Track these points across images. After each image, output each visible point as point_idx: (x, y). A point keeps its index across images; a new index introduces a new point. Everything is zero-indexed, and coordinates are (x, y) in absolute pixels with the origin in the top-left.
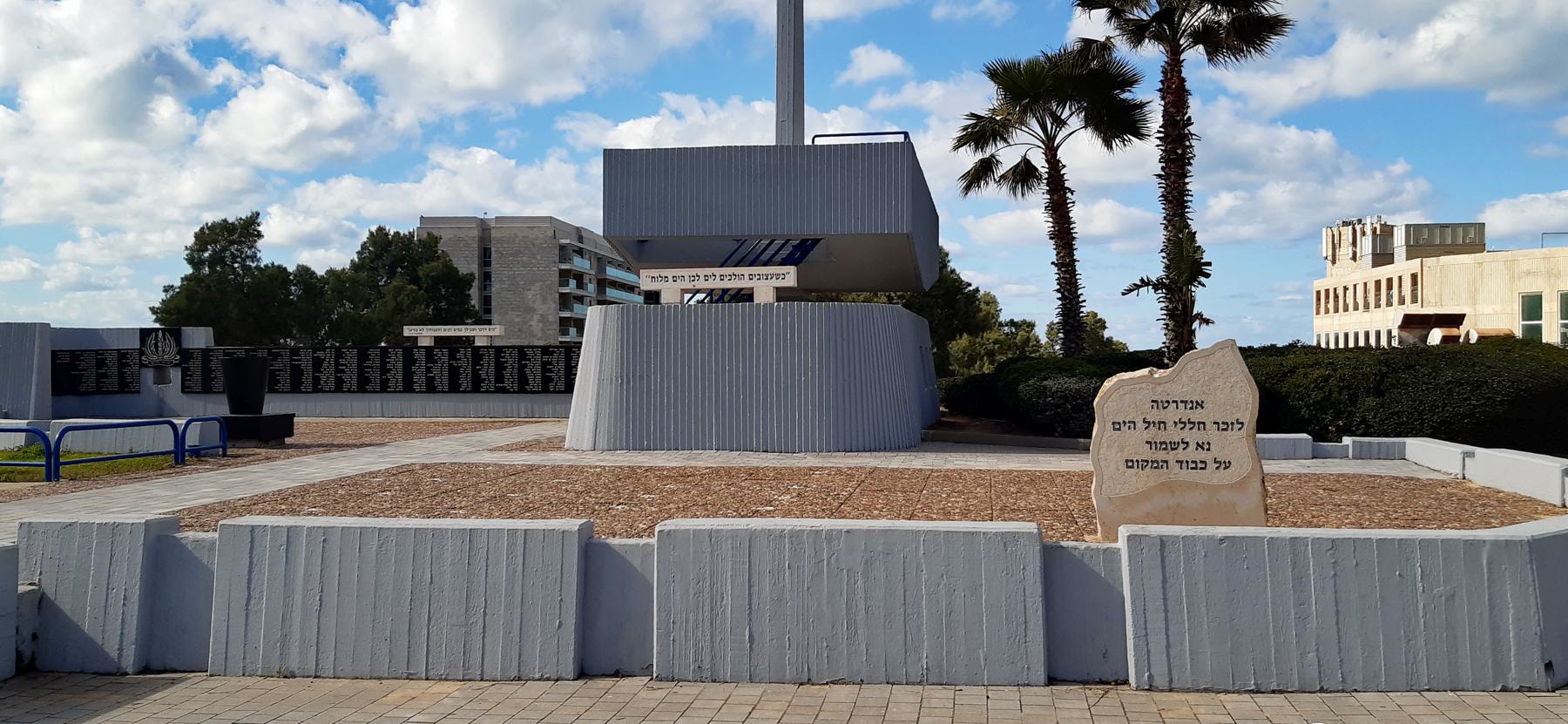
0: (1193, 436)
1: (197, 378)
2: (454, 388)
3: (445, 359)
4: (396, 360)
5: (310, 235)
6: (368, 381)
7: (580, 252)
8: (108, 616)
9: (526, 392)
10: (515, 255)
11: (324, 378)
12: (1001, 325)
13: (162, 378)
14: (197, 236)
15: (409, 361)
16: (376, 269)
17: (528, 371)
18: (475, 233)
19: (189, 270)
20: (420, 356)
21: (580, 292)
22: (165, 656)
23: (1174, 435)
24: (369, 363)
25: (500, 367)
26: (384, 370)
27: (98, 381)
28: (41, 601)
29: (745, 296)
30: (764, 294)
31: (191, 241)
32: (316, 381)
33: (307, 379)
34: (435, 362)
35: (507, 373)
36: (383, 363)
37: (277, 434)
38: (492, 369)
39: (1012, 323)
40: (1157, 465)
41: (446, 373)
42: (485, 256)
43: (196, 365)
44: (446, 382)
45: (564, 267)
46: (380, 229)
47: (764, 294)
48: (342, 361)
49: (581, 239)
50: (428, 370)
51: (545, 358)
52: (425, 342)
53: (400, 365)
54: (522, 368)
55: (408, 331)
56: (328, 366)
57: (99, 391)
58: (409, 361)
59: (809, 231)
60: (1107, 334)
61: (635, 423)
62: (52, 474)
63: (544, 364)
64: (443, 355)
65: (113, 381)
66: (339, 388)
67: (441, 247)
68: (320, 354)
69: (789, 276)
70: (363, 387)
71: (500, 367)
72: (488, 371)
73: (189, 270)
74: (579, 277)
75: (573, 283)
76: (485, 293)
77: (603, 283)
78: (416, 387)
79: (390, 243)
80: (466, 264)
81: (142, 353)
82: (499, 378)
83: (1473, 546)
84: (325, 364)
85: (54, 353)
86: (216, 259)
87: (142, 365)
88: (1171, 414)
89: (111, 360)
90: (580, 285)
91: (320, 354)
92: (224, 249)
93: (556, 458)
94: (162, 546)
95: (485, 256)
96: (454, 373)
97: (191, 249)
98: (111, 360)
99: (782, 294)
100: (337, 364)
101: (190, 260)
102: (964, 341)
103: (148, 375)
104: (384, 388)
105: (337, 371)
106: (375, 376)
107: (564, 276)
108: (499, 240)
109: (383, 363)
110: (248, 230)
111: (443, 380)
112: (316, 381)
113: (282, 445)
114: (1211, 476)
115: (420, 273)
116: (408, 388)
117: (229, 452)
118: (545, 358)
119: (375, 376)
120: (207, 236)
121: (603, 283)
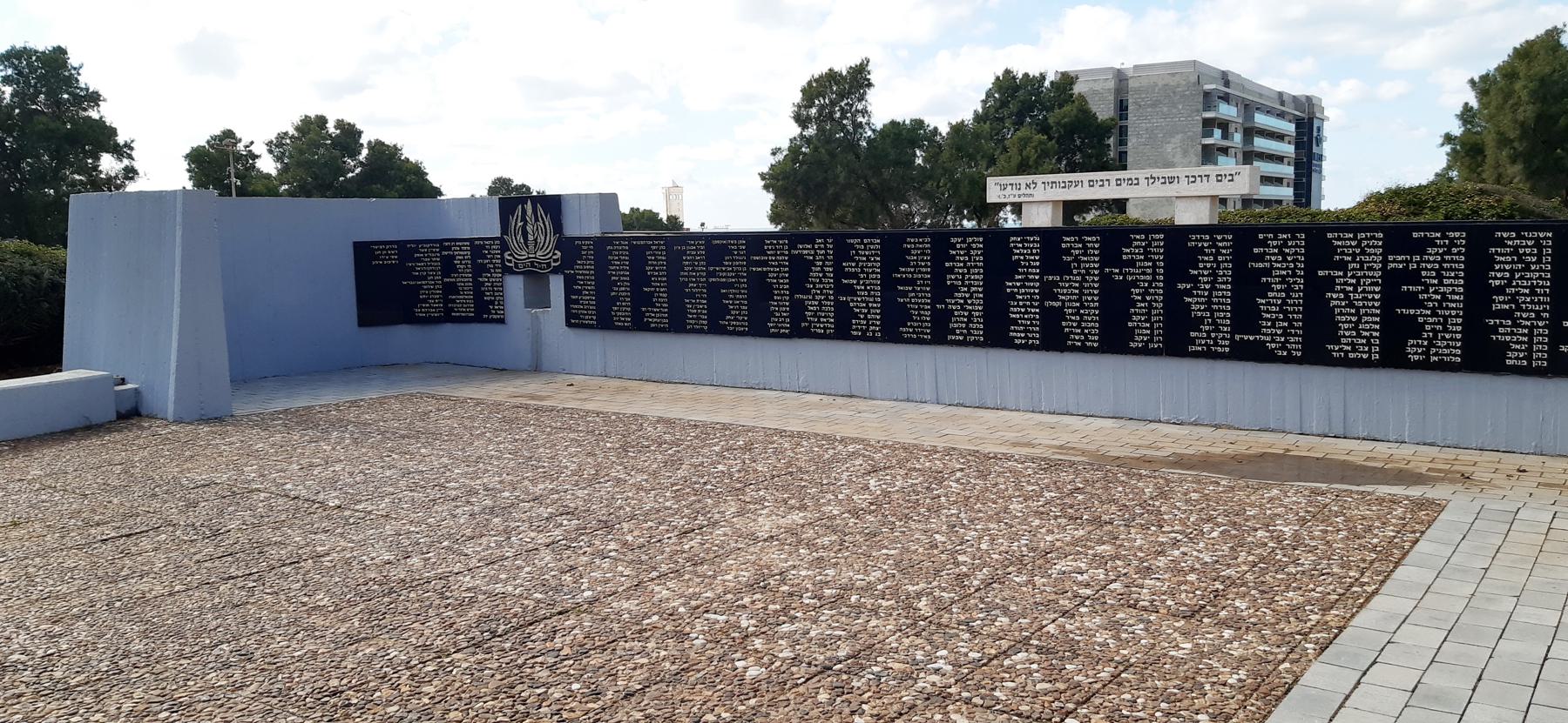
1: (588, 300)
2: (1115, 340)
3: (1093, 262)
6: (904, 315)
7: (1226, 98)
9: (1327, 360)
10: (1154, 105)
11: (812, 306)
13: (538, 299)
14: (804, 91)
16: (1002, 120)
17: (1335, 298)
18: (1111, 85)
19: (795, 130)
20: (1028, 255)
21: (1225, 143)
24: (904, 272)
25: (1248, 285)
26: (942, 290)
27: (446, 301)
32: (798, 310)
33: (780, 307)
34: (1065, 270)
35: (1268, 306)
36: (939, 273)
38: (1225, 290)
41: (1093, 300)
42: (1122, 107)
43: (585, 269)
44: (1093, 325)
45: (1208, 115)
46: (1007, 72)
48: (849, 267)
49: (1227, 84)
50: (1048, 292)
51: (1397, 262)
52: (1042, 217)
53: (977, 277)
54: (1316, 290)
57: (448, 317)
60: (625, 209)
63: (1392, 280)
65: (464, 302)
66: (842, 331)
67: (1077, 89)
68: (805, 250)
70: (893, 329)
71: (1248, 285)
72: (1210, 294)
73: (795, 130)
74: (1224, 126)
75: (1218, 133)
76: (1122, 149)
77: (1250, 132)
78: (1017, 334)
79: (1017, 88)
80: (1104, 111)
81: (504, 247)
82: (1246, 317)
84: (815, 273)
85: (359, 247)
87: (507, 271)
89: (462, 256)
90: (1225, 136)
91: (805, 250)
92: (833, 103)
95: (1122, 107)
96: (1116, 303)
97: (799, 107)
98: (462, 256)
100: (839, 273)
103: (515, 287)
104: (940, 334)
105: (841, 289)
106: (919, 300)
107: (1208, 124)
108: (1138, 91)
109: (939, 273)
110: (857, 80)
112: (798, 310)
115: (1051, 121)
116: (997, 335)
118: (1397, 262)
119: (919, 300)
120: (812, 91)
121: (1250, 132)
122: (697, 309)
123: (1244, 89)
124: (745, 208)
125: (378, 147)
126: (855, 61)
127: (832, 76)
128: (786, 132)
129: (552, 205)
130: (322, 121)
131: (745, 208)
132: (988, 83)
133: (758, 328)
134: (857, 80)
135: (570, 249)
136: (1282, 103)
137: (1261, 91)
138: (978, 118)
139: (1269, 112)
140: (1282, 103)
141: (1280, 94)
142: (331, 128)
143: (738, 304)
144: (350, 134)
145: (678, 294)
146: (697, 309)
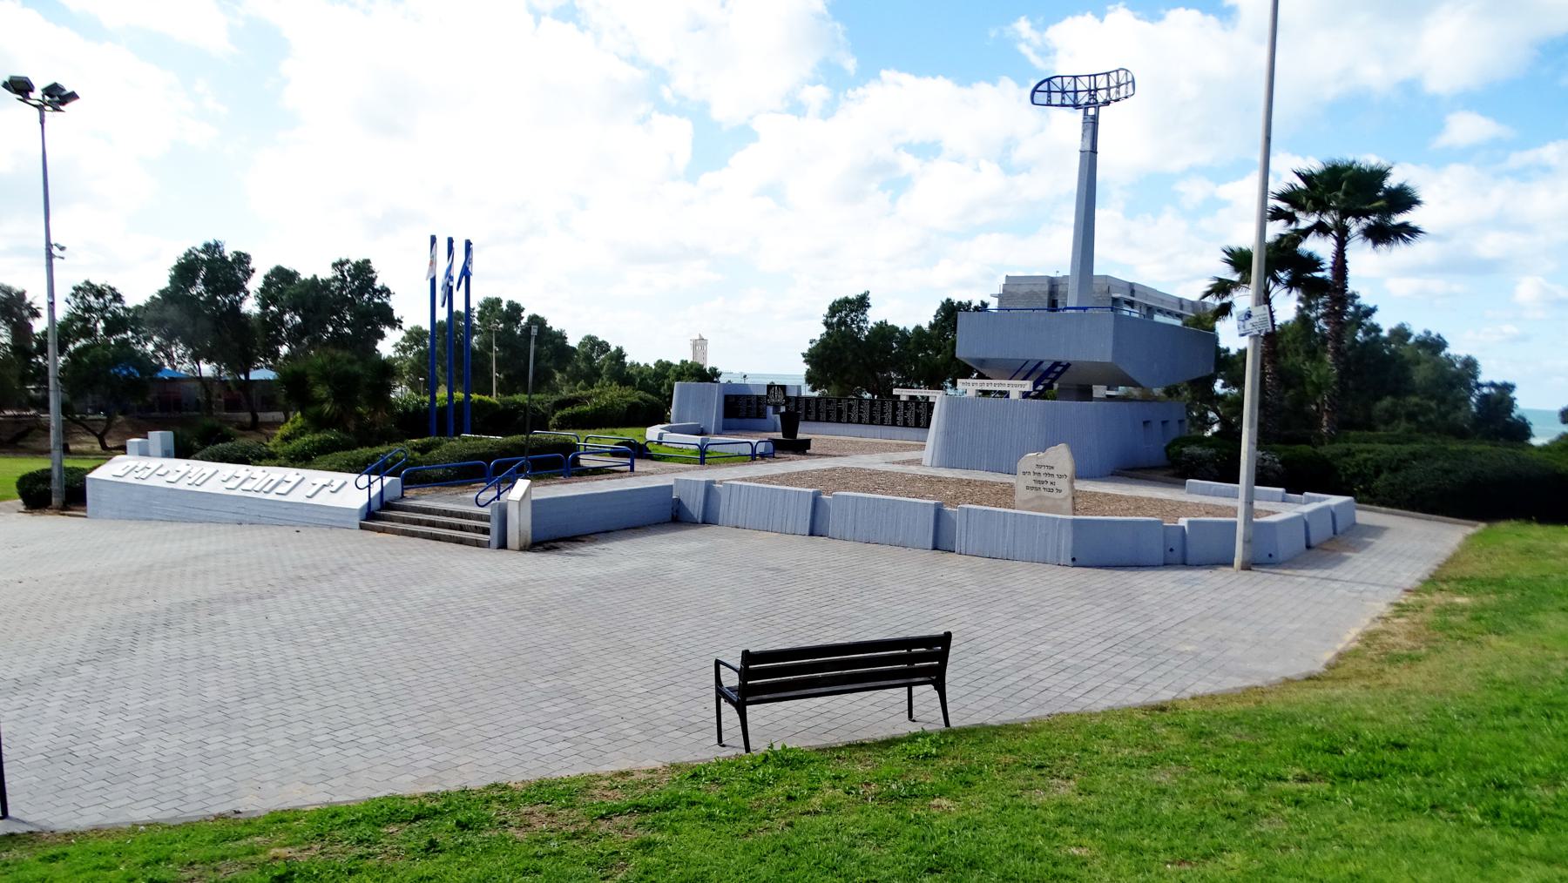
0: (1049, 479)
4: (889, 406)
5: (904, 308)
7: (1131, 304)
8: (695, 507)
12: (1479, 386)
15: (895, 408)
18: (1046, 288)
20: (901, 406)
22: (708, 519)
23: (1043, 478)
26: (883, 413)
28: (679, 501)
29: (1005, 394)
30: (1015, 394)
31: (826, 311)
33: (845, 416)
37: (802, 448)
39: (1493, 385)
40: (1038, 489)
47: (1015, 394)
49: (1133, 293)
52: (903, 398)
55: (895, 392)
56: (855, 409)
57: (747, 417)
58: (895, 408)
59: (1062, 357)
61: (950, 457)
62: (702, 462)
64: (912, 406)
66: (860, 422)
69: (1028, 386)
70: (871, 422)
73: (824, 329)
83: (1055, 519)
86: (842, 322)
88: (1043, 471)
93: (913, 469)
94: (709, 487)
99: (1026, 395)
101: (826, 323)
102: (1387, 402)
103: (770, 409)
104: (882, 423)
110: (862, 303)
111: (912, 421)
113: (804, 453)
114: (1055, 495)
116: (894, 424)
117: (636, 468)
120: (835, 308)
122: (823, 416)
123: (1147, 297)
124: (792, 370)
125: (534, 319)
126: (861, 292)
127: (847, 301)
128: (818, 331)
129: (783, 388)
130: (499, 301)
131: (792, 370)
132: (938, 306)
133: (839, 421)
134: (862, 303)
135: (788, 399)
136: (1182, 307)
137: (1164, 297)
138: (932, 326)
139: (1169, 313)
140: (1182, 307)
141: (1181, 300)
142: (504, 307)
143: (834, 416)
144: (515, 309)
145: (818, 411)
146: (823, 416)
